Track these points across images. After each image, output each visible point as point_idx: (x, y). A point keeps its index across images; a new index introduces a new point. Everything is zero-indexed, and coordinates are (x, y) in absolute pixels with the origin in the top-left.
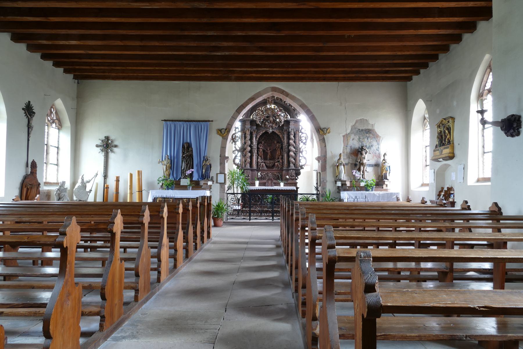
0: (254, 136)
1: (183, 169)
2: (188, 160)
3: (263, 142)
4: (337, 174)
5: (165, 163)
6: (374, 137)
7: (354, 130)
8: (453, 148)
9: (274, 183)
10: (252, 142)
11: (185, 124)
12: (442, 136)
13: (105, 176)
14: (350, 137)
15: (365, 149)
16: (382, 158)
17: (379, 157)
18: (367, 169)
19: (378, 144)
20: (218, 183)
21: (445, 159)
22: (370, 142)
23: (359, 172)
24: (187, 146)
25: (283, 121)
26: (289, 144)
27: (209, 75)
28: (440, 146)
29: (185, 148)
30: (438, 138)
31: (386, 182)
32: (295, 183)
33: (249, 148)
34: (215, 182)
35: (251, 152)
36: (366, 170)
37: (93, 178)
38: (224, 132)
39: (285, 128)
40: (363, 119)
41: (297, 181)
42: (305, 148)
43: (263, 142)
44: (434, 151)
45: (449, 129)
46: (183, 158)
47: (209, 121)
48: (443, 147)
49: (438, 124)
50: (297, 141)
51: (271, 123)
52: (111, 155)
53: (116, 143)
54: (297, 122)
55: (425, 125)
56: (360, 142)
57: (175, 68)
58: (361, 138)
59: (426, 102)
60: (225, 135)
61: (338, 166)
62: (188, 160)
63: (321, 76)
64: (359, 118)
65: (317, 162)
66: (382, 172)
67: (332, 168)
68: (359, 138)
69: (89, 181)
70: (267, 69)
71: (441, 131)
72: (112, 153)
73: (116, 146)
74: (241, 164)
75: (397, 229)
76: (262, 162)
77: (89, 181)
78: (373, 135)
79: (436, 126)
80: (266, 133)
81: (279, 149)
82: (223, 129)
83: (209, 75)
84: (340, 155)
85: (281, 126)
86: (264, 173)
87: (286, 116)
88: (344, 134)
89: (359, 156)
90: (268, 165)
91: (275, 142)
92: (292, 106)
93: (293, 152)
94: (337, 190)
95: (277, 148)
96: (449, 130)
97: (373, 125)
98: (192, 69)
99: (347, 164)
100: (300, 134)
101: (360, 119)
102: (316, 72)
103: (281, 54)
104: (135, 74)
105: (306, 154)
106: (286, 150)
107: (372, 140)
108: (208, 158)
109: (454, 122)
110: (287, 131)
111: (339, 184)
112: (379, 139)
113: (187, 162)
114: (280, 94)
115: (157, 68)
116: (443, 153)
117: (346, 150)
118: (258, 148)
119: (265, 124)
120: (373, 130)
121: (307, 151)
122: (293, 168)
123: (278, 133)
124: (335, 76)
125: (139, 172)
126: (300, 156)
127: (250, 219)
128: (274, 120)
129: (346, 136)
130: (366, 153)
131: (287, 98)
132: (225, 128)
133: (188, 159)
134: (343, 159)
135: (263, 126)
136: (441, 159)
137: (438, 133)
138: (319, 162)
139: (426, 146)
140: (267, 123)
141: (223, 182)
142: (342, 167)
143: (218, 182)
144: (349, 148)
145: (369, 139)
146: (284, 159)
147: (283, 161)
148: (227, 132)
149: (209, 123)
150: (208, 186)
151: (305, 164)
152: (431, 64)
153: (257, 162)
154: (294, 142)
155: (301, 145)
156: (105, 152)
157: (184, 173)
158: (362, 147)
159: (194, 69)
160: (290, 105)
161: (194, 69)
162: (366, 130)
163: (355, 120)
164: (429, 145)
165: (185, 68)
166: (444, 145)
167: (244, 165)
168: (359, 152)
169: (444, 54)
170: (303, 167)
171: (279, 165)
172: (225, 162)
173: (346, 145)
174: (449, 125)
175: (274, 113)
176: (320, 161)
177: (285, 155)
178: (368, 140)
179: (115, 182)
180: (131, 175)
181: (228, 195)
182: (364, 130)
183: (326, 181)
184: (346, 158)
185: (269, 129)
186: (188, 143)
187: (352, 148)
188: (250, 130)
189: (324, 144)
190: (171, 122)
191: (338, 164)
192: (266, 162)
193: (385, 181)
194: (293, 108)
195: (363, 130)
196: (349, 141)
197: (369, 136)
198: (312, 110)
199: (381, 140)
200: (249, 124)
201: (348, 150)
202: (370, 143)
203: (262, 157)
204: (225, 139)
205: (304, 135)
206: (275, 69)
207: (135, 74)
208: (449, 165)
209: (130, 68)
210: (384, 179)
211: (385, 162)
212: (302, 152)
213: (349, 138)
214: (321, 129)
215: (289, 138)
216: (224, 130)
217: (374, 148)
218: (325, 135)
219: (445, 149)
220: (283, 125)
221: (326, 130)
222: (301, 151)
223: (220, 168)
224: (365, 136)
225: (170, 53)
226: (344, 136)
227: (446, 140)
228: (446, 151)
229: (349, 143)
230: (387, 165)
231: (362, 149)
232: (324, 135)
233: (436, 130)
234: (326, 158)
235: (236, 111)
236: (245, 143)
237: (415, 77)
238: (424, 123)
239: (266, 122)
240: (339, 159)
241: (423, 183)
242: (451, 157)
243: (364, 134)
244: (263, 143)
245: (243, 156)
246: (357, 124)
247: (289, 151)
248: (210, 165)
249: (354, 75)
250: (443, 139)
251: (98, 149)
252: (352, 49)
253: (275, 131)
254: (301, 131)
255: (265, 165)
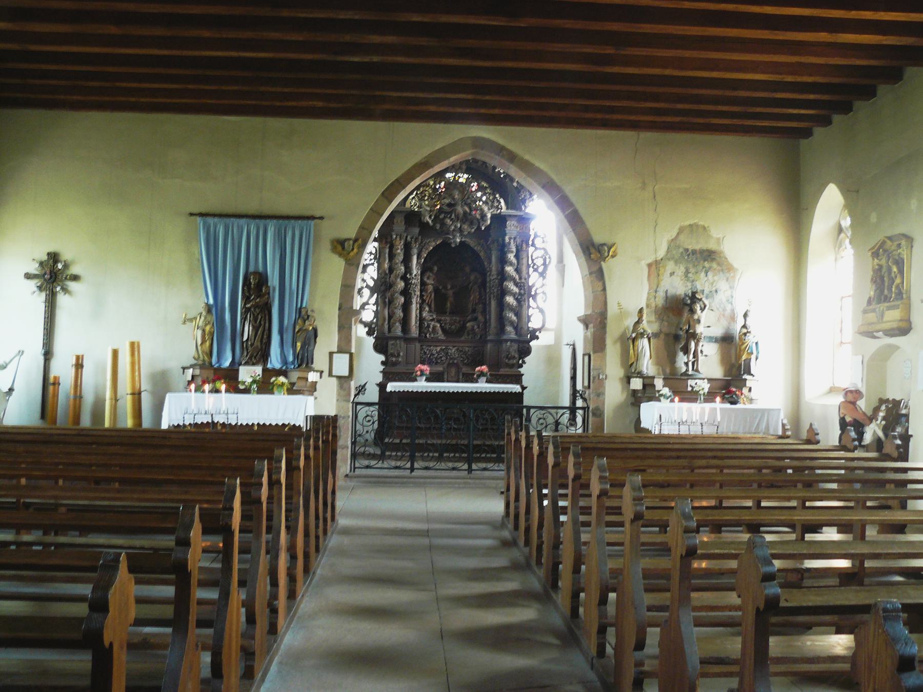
0: (415, 251)
1: (245, 338)
2: (260, 317)
3: (436, 268)
4: (632, 360)
5: (201, 324)
6: (722, 270)
7: (674, 252)
8: (908, 308)
9: (464, 374)
10: (408, 269)
11: (261, 223)
12: (882, 278)
13: (48, 355)
14: (664, 267)
15: (701, 300)
16: (740, 322)
17: (733, 318)
18: (703, 349)
19: (731, 287)
20: (334, 376)
21: (890, 333)
22: (712, 281)
23: (685, 355)
24: (257, 281)
25: (489, 216)
26: (503, 276)
27: (320, 104)
28: (879, 302)
29: (252, 286)
30: (874, 282)
31: (750, 381)
32: (516, 375)
33: (401, 285)
34: (326, 374)
35: (406, 293)
36: (702, 352)
37: (14, 358)
38: (351, 247)
39: (492, 232)
40: (697, 225)
41: (522, 370)
42: (543, 285)
43: (436, 268)
44: (865, 312)
45: (900, 263)
46: (246, 311)
47: (312, 218)
48: (886, 304)
49: (873, 248)
50: (524, 268)
51: (457, 221)
52: (62, 300)
53: (74, 270)
54: (524, 220)
55: (840, 246)
56: (688, 281)
57: (236, 88)
58: (692, 270)
59: (846, 191)
60: (352, 254)
61: (634, 340)
62: (260, 317)
63: (599, 116)
64: (687, 223)
65: (581, 326)
66: (739, 357)
67: (618, 346)
68: (687, 272)
69: (5, 365)
70: (470, 97)
71: (881, 267)
72: (65, 294)
73: (75, 278)
74: (380, 323)
75: (808, 504)
76: (432, 320)
77: (5, 365)
78: (719, 264)
79: (870, 253)
80: (445, 245)
81: (476, 287)
82: (349, 239)
83: (320, 104)
84: (641, 311)
85: (483, 228)
86: (439, 349)
87: (496, 204)
88: (650, 261)
89: (686, 314)
90: (447, 327)
91: (467, 269)
92: (512, 180)
93: (514, 296)
94: (633, 400)
95: (471, 285)
96: (900, 265)
97: (718, 239)
98: (279, 89)
99: (656, 335)
100: (531, 249)
101: (690, 225)
102: (586, 108)
103: (510, 64)
104: (133, 99)
105: (545, 301)
106: (496, 290)
107: (716, 278)
108: (310, 313)
109: (912, 247)
110: (498, 241)
111: (636, 384)
112: (732, 274)
113: (256, 322)
114: (492, 155)
115: (190, 87)
116: (885, 319)
117: (653, 299)
118: (423, 284)
119: (443, 224)
120: (721, 253)
121: (548, 295)
122: (513, 336)
123: (475, 246)
124: (633, 118)
125: (132, 344)
126: (529, 307)
127: (412, 469)
128: (465, 212)
129: (654, 267)
130: (702, 310)
131: (511, 165)
132: (353, 236)
133: (258, 314)
134: (648, 322)
135: (438, 228)
136: (881, 333)
137: (874, 271)
138: (587, 327)
139: (843, 297)
140: (448, 221)
141: (346, 373)
142: (645, 341)
143: (333, 374)
144: (661, 294)
145: (710, 274)
146: (490, 312)
147: (486, 318)
148: (358, 248)
149: (312, 223)
150: (308, 384)
151: (543, 326)
152: (857, 104)
153: (421, 320)
154: (517, 270)
155: (534, 279)
156: (48, 292)
157: (247, 350)
158: (694, 294)
159: (286, 90)
160: (507, 176)
161: (286, 90)
162: (702, 252)
163: (678, 226)
164: (850, 294)
165: (262, 89)
166: (887, 299)
167: (386, 327)
168: (687, 305)
169: (888, 87)
170: (537, 334)
171: (476, 327)
172: (351, 324)
173: (655, 287)
174: (899, 254)
175: (466, 197)
176: (591, 326)
177: (493, 304)
178: (706, 276)
179: (73, 370)
180: (115, 353)
181: (359, 407)
182: (698, 252)
183: (604, 377)
184: (653, 318)
185: (454, 237)
186: (260, 274)
187: (668, 294)
188: (404, 237)
189: (601, 284)
190: (216, 220)
191: (634, 335)
192: (443, 318)
193: (746, 380)
194: (515, 184)
195: (696, 250)
196: (661, 277)
197: (710, 268)
198: (573, 199)
199: (738, 278)
200: (401, 222)
201: (660, 301)
202: (712, 284)
203: (433, 306)
204: (353, 265)
205: (540, 253)
206: (488, 98)
207: (133, 99)
208: (898, 348)
209: (124, 85)
210: (744, 374)
211: (748, 332)
212: (534, 297)
213: (662, 270)
214: (593, 245)
215: (503, 261)
216: (351, 242)
217: (721, 297)
218: (604, 261)
219: (889, 310)
220: (488, 228)
221: (606, 248)
222: (533, 293)
223: (340, 340)
224: (701, 268)
225: (234, 54)
226: (650, 265)
227: (893, 290)
228: (893, 316)
229: (662, 283)
230: (750, 339)
231: (694, 298)
232: (602, 263)
233: (870, 264)
234: (606, 318)
235: (383, 194)
236: (391, 270)
237: (818, 132)
238: (838, 241)
239: (445, 217)
240: (638, 322)
241: (832, 385)
242: (904, 329)
243: (699, 262)
244: (435, 272)
245: (384, 302)
246: (682, 237)
247: (503, 292)
248: (315, 331)
249: (678, 119)
250: (886, 284)
251: (33, 284)
252: (681, 63)
253: (468, 240)
254: (533, 241)
255: (441, 326)
